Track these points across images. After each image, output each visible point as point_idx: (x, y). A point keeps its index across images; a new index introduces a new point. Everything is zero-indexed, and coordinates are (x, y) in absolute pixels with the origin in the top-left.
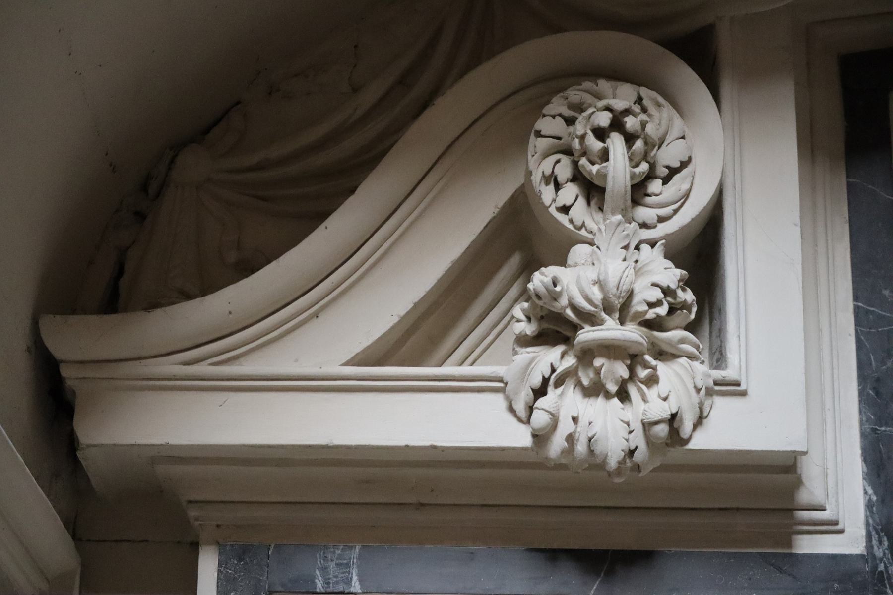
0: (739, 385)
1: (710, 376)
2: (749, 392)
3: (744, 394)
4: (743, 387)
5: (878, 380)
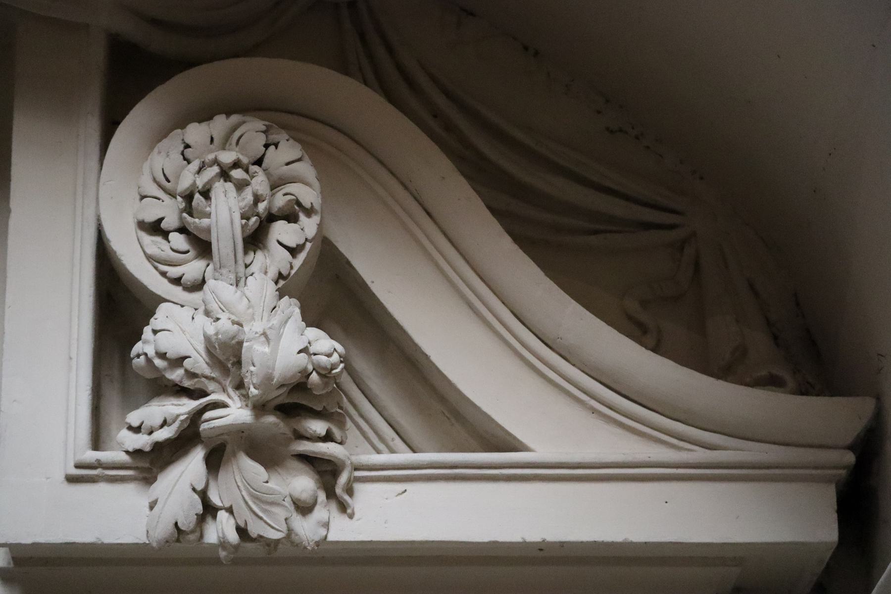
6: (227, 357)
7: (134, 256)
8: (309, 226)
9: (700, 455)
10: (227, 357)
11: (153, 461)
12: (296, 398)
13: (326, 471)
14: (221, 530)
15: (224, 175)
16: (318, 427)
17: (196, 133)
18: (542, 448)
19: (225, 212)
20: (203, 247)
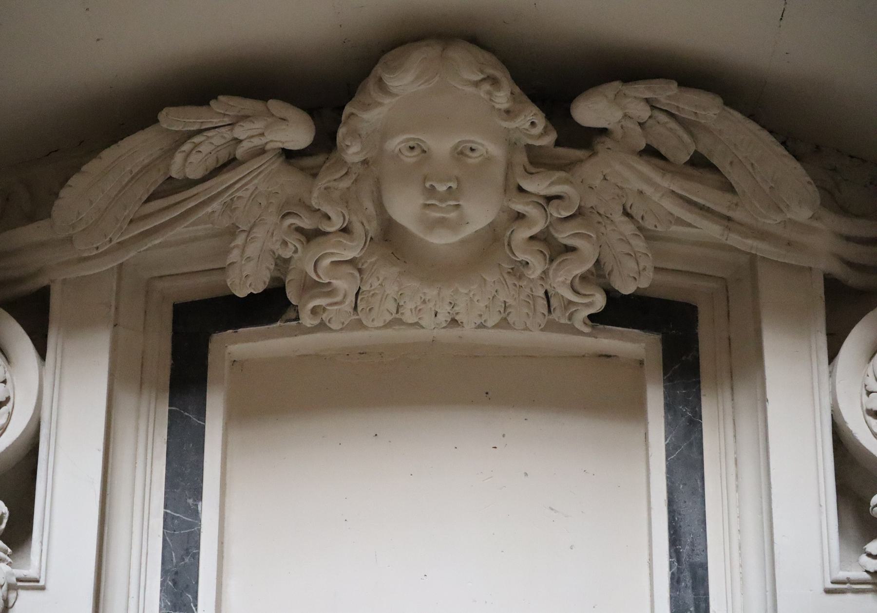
0: (38, 581)
1: (13, 575)
2: (48, 587)
3: (43, 588)
4: (42, 583)
5: (176, 573)
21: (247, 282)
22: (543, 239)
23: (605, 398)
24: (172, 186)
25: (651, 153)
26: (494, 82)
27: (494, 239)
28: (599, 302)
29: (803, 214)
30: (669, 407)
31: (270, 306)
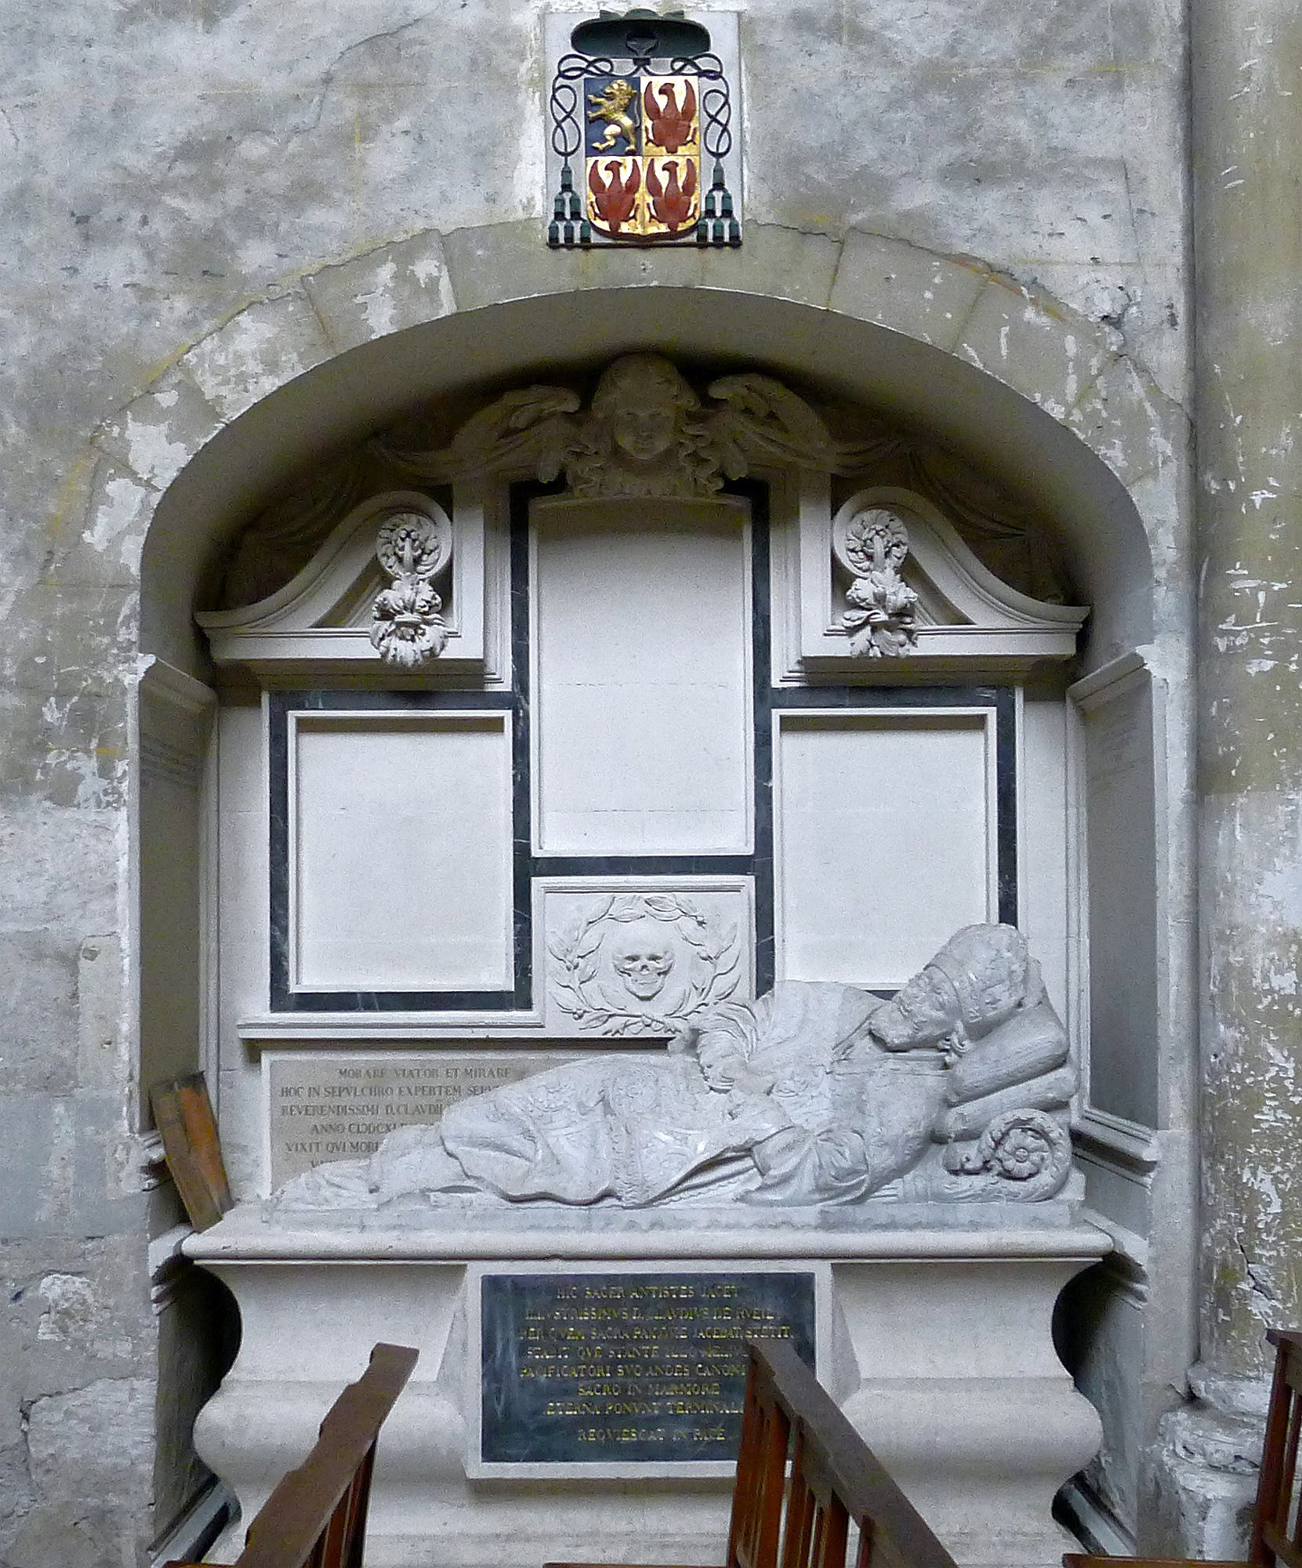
6: (881, 599)
7: (845, 559)
8: (905, 549)
9: (1032, 625)
10: (881, 599)
11: (852, 631)
12: (903, 613)
13: (910, 633)
14: (875, 652)
15: (877, 533)
16: (908, 620)
17: (867, 516)
18: (980, 624)
19: (879, 547)
20: (870, 557)
21: (547, 475)
22: (694, 454)
23: (719, 529)
24: (508, 433)
25: (747, 411)
26: (669, 381)
27: (669, 454)
28: (721, 485)
29: (822, 445)
30: (754, 531)
31: (559, 485)
